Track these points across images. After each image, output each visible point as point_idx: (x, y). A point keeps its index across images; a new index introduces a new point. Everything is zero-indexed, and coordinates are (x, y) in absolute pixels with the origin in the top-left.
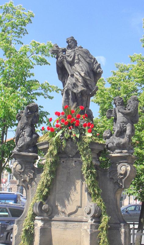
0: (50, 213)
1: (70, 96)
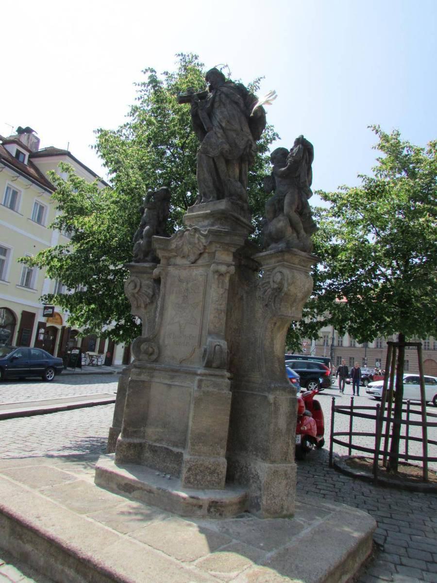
0: (154, 357)
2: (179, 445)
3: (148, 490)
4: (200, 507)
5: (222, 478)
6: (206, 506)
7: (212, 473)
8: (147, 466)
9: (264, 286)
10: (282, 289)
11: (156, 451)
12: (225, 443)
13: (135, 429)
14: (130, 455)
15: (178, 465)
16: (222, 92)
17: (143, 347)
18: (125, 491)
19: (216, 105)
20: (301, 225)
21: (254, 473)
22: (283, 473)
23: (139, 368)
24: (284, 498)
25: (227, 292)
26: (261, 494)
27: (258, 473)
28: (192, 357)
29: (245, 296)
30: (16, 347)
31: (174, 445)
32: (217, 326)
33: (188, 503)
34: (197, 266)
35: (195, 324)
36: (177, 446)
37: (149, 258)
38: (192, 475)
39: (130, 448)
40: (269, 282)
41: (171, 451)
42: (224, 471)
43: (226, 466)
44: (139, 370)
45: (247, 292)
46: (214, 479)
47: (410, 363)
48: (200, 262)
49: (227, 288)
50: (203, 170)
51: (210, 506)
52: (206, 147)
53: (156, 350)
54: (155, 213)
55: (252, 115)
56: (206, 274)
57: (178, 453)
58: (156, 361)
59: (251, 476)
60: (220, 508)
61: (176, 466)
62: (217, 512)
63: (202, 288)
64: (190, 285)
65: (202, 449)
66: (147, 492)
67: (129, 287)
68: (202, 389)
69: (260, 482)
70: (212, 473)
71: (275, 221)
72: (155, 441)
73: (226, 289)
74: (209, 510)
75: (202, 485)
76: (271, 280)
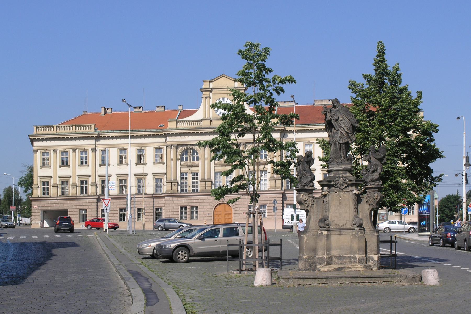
1: (338, 146)
36: (347, 254)
47: (198, 210)
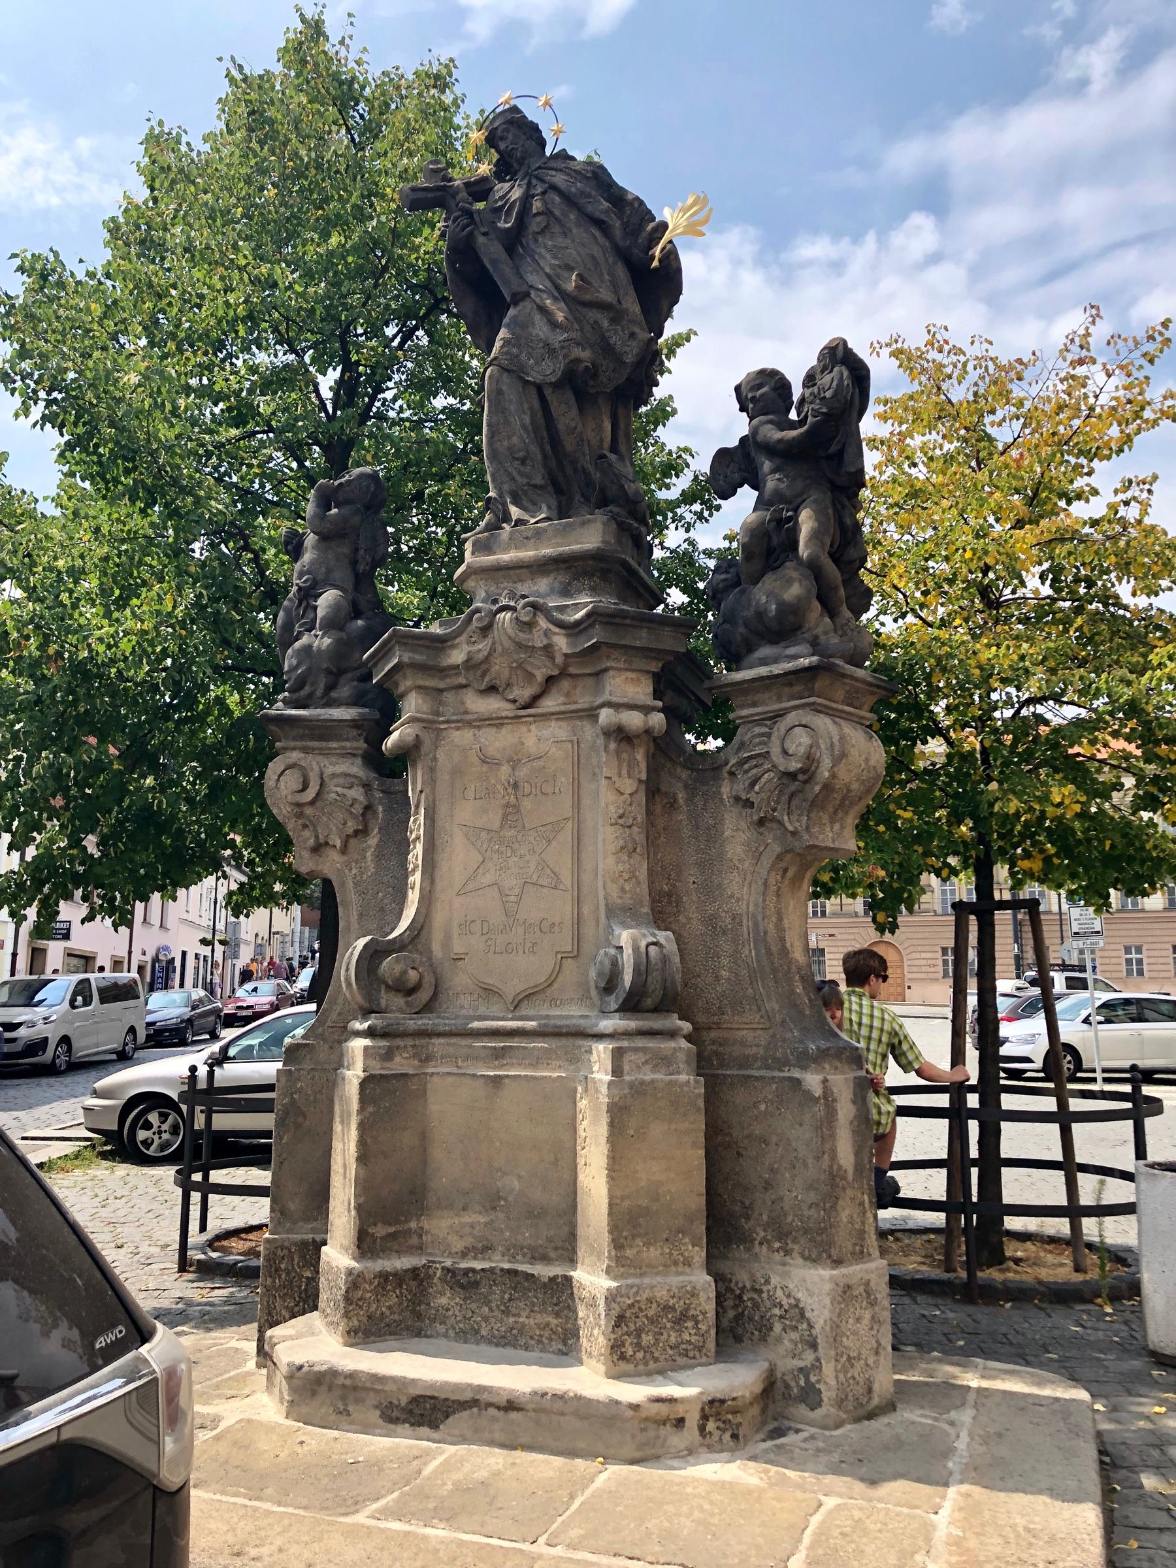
0: (423, 996)
2: (552, 1254)
3: (504, 1404)
4: (680, 1422)
5: (708, 1331)
6: (693, 1420)
7: (682, 1318)
8: (446, 1336)
9: (746, 767)
10: (814, 773)
11: (476, 1284)
12: (701, 1228)
13: (391, 1230)
14: (388, 1313)
15: (557, 1315)
16: (553, 187)
17: (389, 966)
18: (412, 1425)
19: (535, 224)
20: (842, 592)
21: (785, 1302)
22: (861, 1289)
23: (384, 1035)
24: (871, 1361)
25: (643, 787)
26: (818, 1360)
27: (798, 1300)
28: (556, 985)
29: (681, 796)
30: (1066, 991)
31: (533, 1258)
32: (627, 888)
33: (647, 1419)
34: (542, 715)
35: (555, 888)
36: (545, 1259)
37: (345, 690)
38: (627, 1334)
39: (384, 1289)
40: (766, 755)
41: (529, 1277)
42: (711, 1307)
43: (713, 1295)
44: (383, 1043)
45: (686, 787)
46: (686, 1337)
47: (827, 956)
48: (550, 704)
49: (644, 777)
50: (507, 422)
51: (705, 1417)
52: (515, 350)
53: (429, 979)
54: (346, 550)
55: (655, 263)
56: (575, 739)
57: (553, 1280)
58: (427, 1008)
59: (777, 1311)
60: (730, 1417)
61: (554, 1321)
62: (724, 1431)
63: (564, 781)
64: (522, 772)
65: (645, 1255)
66: (499, 1408)
67: (282, 784)
68: (627, 1078)
69: (811, 1326)
70: (682, 1318)
71: (769, 582)
72: (464, 1255)
73: (640, 781)
74: (702, 1429)
75: (656, 1360)
76: (775, 750)
